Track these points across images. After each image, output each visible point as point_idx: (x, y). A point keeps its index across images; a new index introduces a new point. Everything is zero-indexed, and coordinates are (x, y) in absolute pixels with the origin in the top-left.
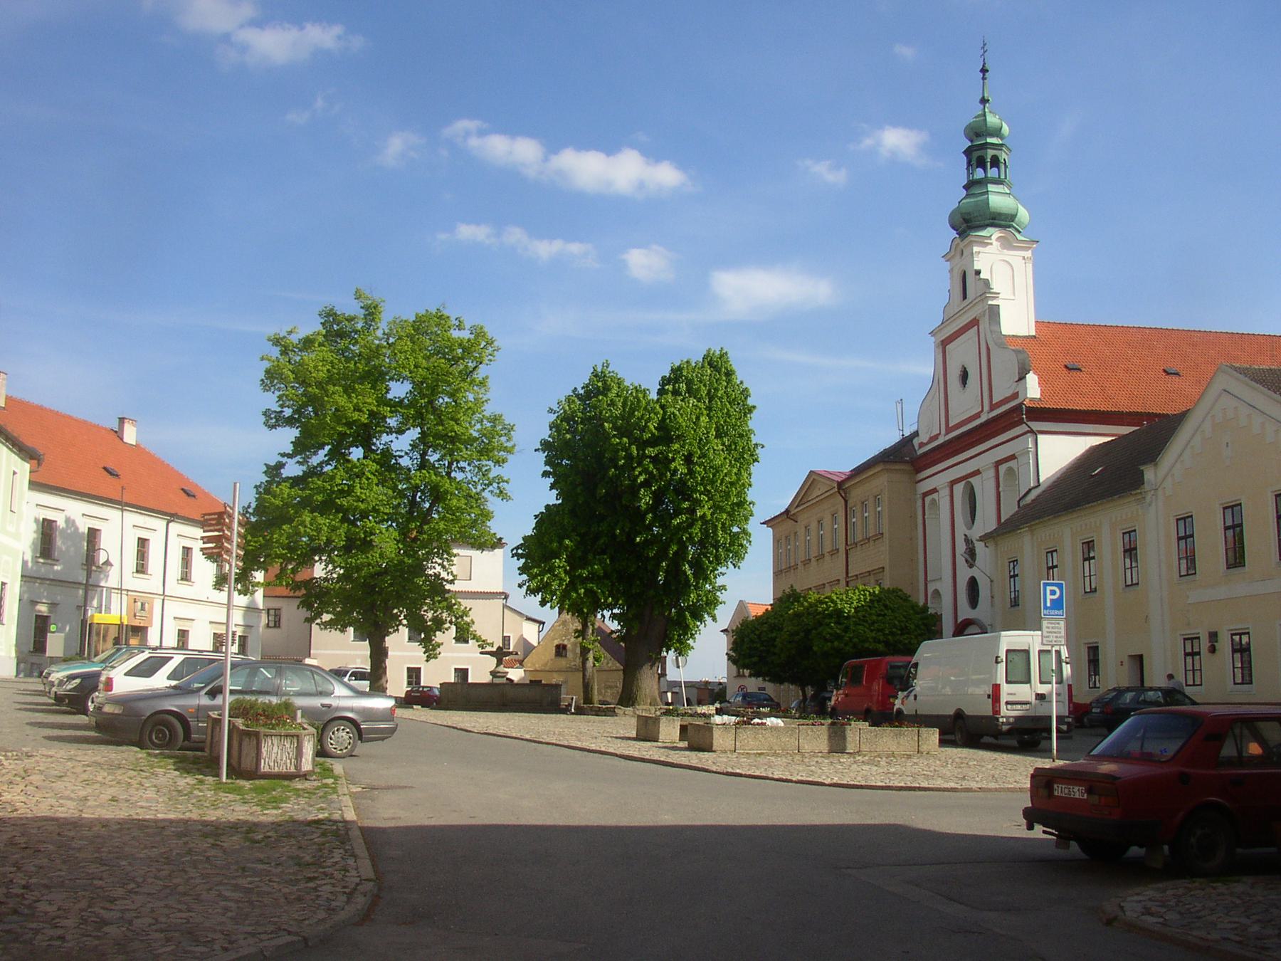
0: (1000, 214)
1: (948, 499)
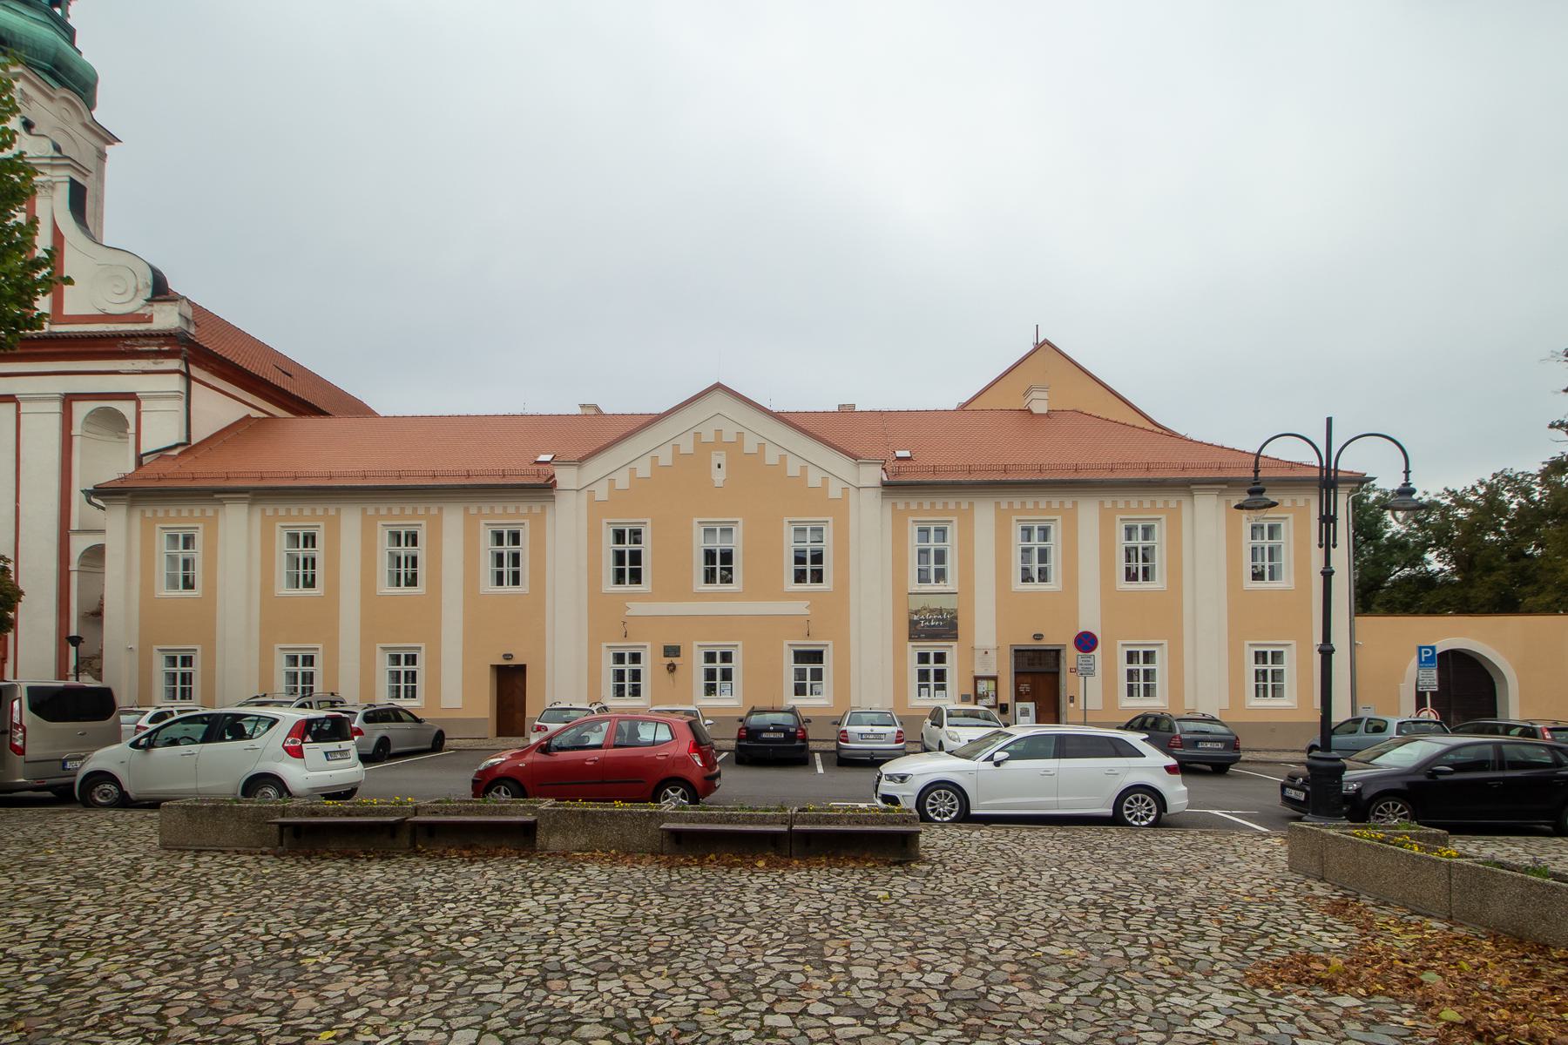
1: (56, 421)
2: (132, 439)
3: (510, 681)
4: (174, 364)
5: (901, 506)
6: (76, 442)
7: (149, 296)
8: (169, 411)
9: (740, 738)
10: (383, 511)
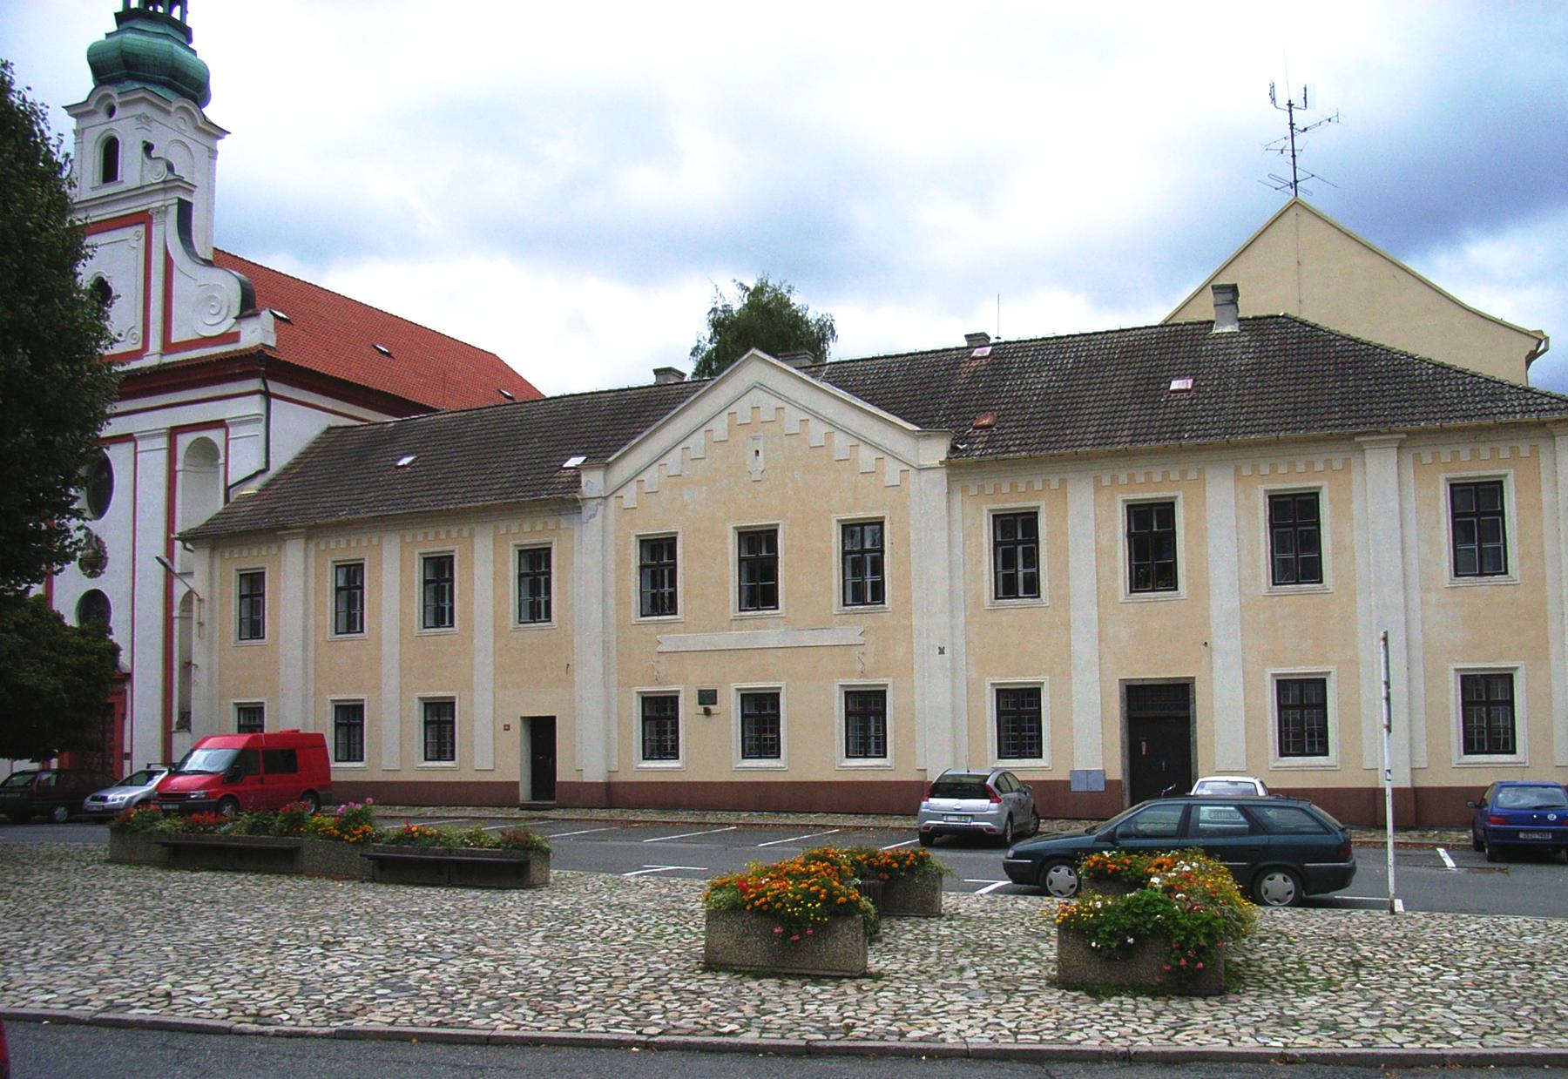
0: (185, 75)
1: (162, 457)
2: (222, 469)
3: (541, 733)
4: (256, 384)
5: (1246, 471)
6: (180, 476)
7: (237, 313)
8: (271, 435)
9: (1350, 872)
10: (515, 529)
